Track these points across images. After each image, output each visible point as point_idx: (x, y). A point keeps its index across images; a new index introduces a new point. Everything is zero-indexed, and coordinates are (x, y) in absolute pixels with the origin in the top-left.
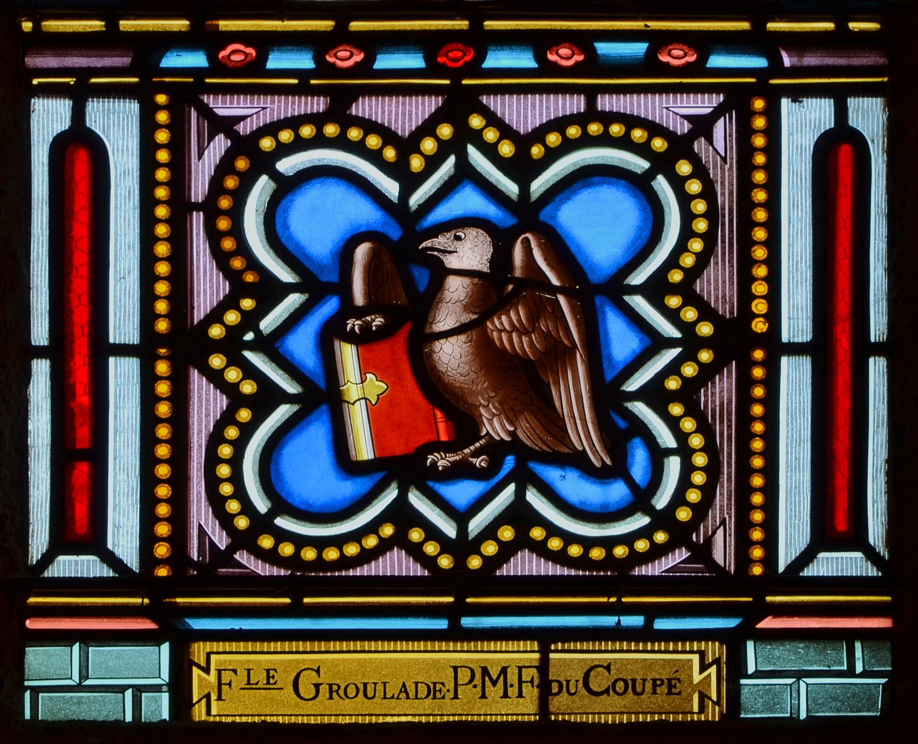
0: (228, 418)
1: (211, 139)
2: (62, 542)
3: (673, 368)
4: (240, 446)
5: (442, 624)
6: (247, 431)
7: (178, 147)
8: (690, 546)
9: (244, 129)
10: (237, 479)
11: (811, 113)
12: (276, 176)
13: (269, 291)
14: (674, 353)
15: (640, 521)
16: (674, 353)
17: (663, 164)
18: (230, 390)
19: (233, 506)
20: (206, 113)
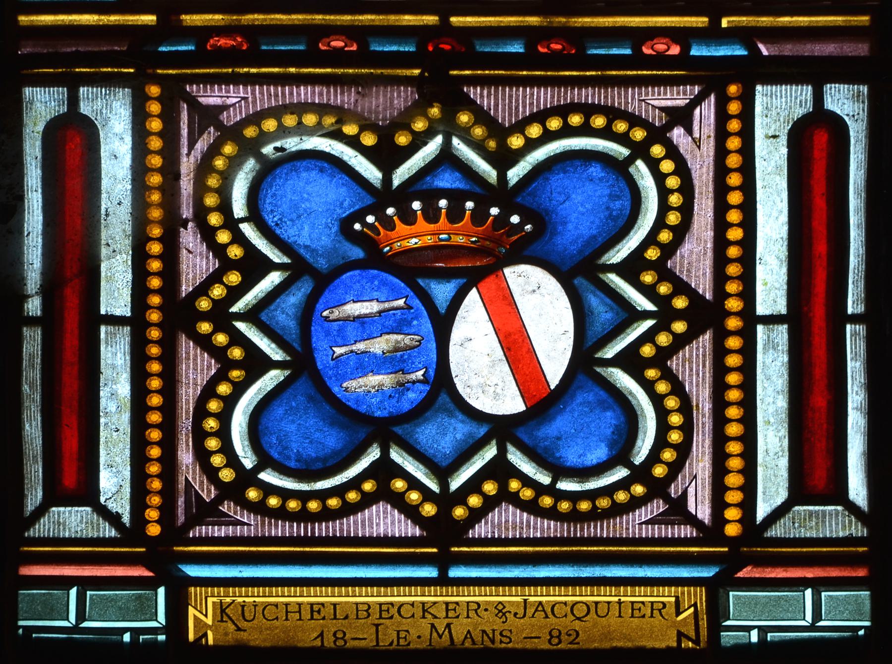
0: (669, 250)
1: (201, 134)
2: (56, 495)
3: (648, 337)
4: (660, 224)
5: (430, 572)
6: (651, 240)
7: (170, 135)
8: (667, 498)
9: (658, 506)
10: (663, 193)
11: (787, 102)
12: (629, 465)
13: (254, 266)
14: (649, 323)
15: (621, 473)
16: (649, 323)
17: (640, 151)
18: (665, 275)
19: (667, 166)
20: (193, 104)
